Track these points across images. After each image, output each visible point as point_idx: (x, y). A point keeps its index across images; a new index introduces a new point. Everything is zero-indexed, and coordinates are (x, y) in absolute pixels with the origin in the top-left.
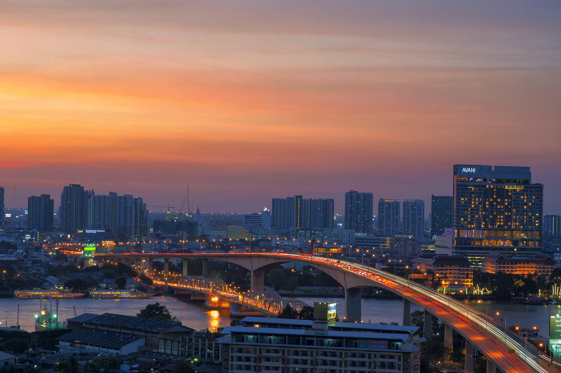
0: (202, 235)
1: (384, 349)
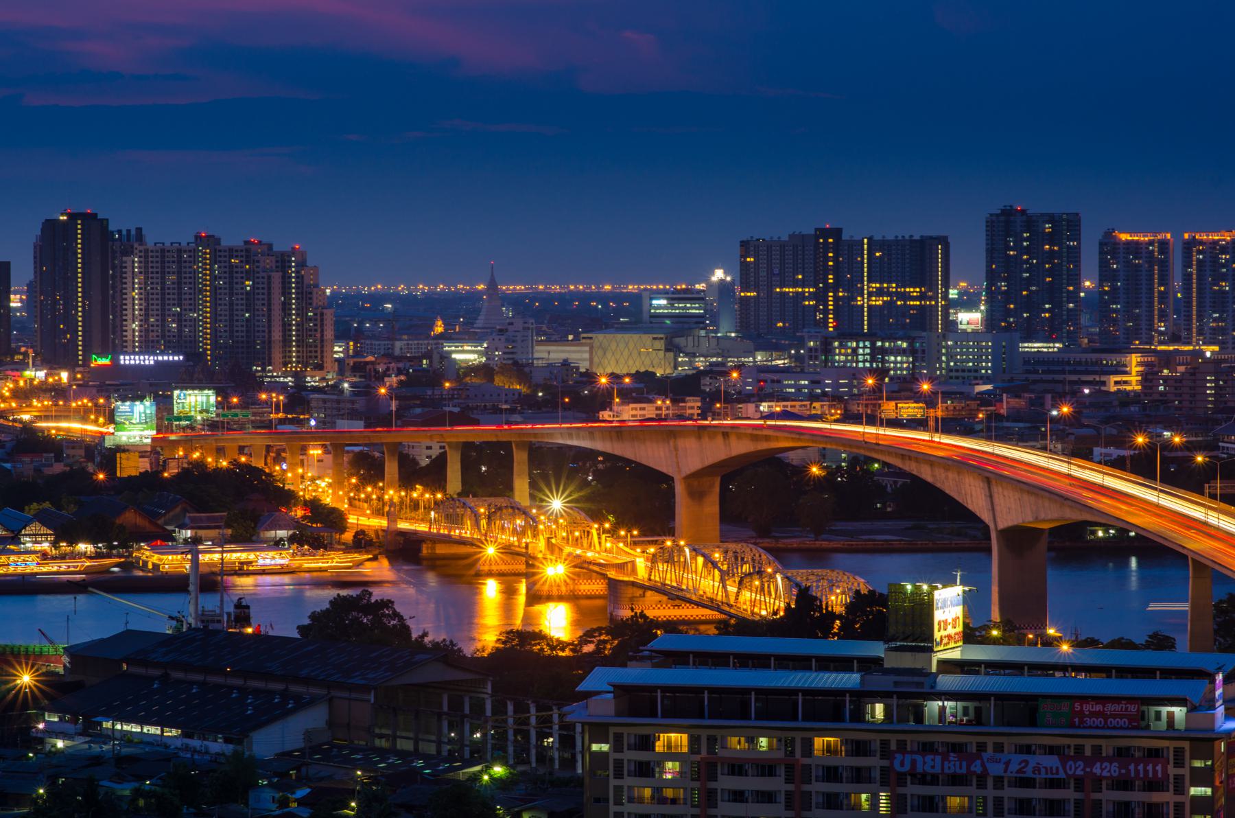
0: (510, 362)
1: (1127, 728)
